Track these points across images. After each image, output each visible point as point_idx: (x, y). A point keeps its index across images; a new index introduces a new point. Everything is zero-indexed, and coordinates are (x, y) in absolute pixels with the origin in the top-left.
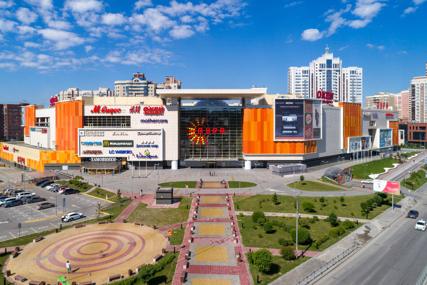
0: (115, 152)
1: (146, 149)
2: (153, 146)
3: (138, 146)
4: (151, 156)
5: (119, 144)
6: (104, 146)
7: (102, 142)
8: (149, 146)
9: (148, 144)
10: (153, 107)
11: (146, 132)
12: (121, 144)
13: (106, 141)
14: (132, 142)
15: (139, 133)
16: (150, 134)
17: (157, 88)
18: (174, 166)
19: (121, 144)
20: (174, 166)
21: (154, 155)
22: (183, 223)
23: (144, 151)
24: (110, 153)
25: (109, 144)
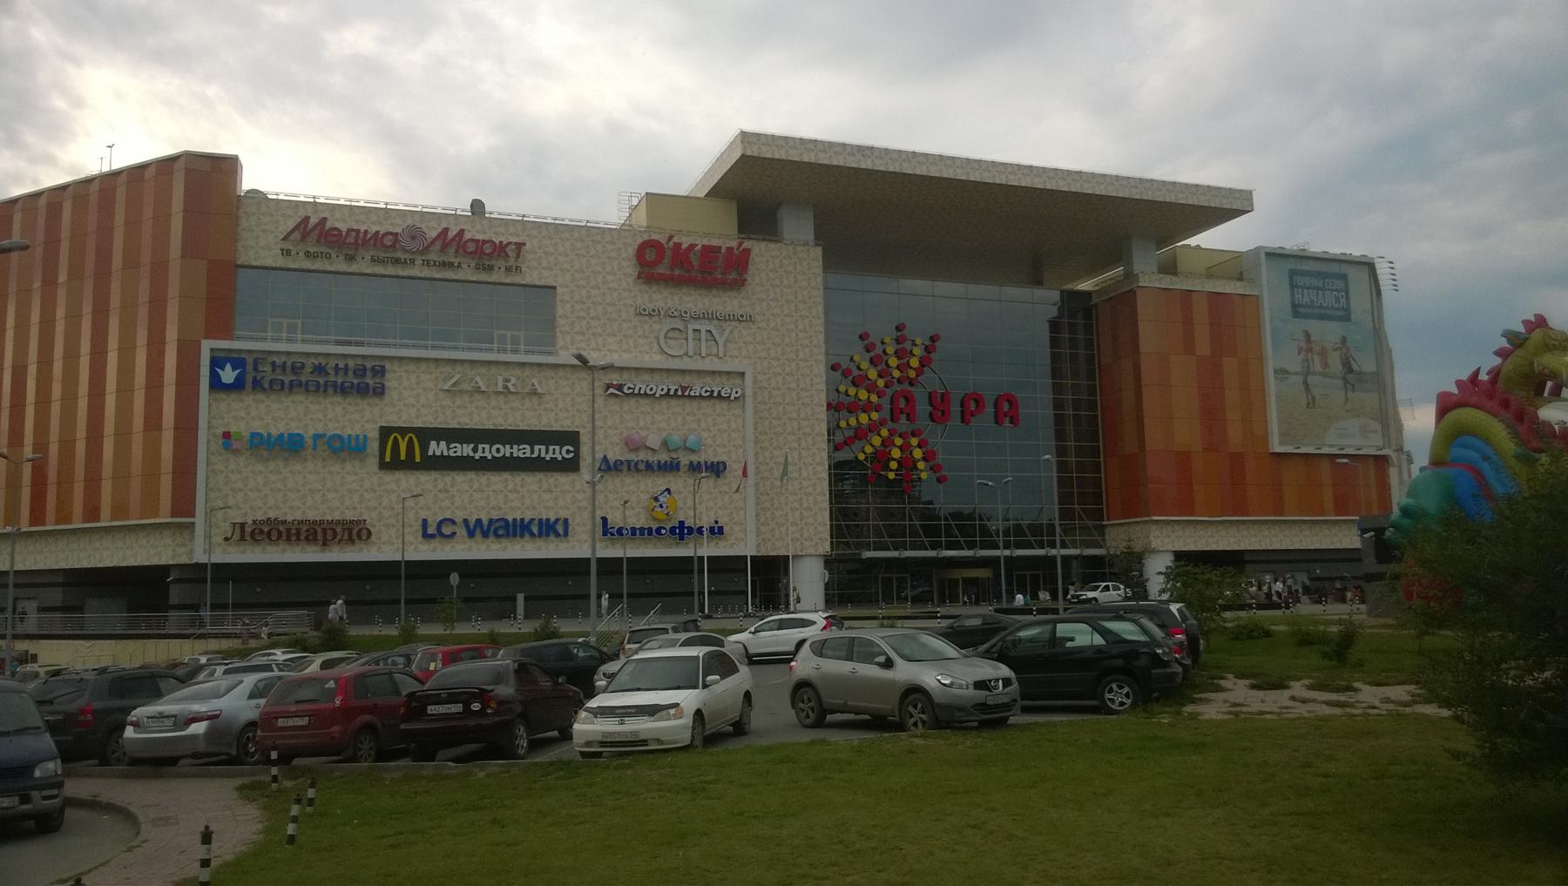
1: (659, 483)
3: (609, 467)
4: (690, 530)
5: (487, 451)
6: (383, 466)
8: (671, 467)
9: (664, 457)
10: (692, 246)
12: (506, 451)
13: (403, 431)
14: (571, 438)
15: (620, 387)
16: (682, 395)
18: (808, 581)
19: (506, 451)
20: (808, 581)
21: (706, 522)
22: (302, 630)
23: (644, 497)
24: (426, 535)
25: (424, 449)
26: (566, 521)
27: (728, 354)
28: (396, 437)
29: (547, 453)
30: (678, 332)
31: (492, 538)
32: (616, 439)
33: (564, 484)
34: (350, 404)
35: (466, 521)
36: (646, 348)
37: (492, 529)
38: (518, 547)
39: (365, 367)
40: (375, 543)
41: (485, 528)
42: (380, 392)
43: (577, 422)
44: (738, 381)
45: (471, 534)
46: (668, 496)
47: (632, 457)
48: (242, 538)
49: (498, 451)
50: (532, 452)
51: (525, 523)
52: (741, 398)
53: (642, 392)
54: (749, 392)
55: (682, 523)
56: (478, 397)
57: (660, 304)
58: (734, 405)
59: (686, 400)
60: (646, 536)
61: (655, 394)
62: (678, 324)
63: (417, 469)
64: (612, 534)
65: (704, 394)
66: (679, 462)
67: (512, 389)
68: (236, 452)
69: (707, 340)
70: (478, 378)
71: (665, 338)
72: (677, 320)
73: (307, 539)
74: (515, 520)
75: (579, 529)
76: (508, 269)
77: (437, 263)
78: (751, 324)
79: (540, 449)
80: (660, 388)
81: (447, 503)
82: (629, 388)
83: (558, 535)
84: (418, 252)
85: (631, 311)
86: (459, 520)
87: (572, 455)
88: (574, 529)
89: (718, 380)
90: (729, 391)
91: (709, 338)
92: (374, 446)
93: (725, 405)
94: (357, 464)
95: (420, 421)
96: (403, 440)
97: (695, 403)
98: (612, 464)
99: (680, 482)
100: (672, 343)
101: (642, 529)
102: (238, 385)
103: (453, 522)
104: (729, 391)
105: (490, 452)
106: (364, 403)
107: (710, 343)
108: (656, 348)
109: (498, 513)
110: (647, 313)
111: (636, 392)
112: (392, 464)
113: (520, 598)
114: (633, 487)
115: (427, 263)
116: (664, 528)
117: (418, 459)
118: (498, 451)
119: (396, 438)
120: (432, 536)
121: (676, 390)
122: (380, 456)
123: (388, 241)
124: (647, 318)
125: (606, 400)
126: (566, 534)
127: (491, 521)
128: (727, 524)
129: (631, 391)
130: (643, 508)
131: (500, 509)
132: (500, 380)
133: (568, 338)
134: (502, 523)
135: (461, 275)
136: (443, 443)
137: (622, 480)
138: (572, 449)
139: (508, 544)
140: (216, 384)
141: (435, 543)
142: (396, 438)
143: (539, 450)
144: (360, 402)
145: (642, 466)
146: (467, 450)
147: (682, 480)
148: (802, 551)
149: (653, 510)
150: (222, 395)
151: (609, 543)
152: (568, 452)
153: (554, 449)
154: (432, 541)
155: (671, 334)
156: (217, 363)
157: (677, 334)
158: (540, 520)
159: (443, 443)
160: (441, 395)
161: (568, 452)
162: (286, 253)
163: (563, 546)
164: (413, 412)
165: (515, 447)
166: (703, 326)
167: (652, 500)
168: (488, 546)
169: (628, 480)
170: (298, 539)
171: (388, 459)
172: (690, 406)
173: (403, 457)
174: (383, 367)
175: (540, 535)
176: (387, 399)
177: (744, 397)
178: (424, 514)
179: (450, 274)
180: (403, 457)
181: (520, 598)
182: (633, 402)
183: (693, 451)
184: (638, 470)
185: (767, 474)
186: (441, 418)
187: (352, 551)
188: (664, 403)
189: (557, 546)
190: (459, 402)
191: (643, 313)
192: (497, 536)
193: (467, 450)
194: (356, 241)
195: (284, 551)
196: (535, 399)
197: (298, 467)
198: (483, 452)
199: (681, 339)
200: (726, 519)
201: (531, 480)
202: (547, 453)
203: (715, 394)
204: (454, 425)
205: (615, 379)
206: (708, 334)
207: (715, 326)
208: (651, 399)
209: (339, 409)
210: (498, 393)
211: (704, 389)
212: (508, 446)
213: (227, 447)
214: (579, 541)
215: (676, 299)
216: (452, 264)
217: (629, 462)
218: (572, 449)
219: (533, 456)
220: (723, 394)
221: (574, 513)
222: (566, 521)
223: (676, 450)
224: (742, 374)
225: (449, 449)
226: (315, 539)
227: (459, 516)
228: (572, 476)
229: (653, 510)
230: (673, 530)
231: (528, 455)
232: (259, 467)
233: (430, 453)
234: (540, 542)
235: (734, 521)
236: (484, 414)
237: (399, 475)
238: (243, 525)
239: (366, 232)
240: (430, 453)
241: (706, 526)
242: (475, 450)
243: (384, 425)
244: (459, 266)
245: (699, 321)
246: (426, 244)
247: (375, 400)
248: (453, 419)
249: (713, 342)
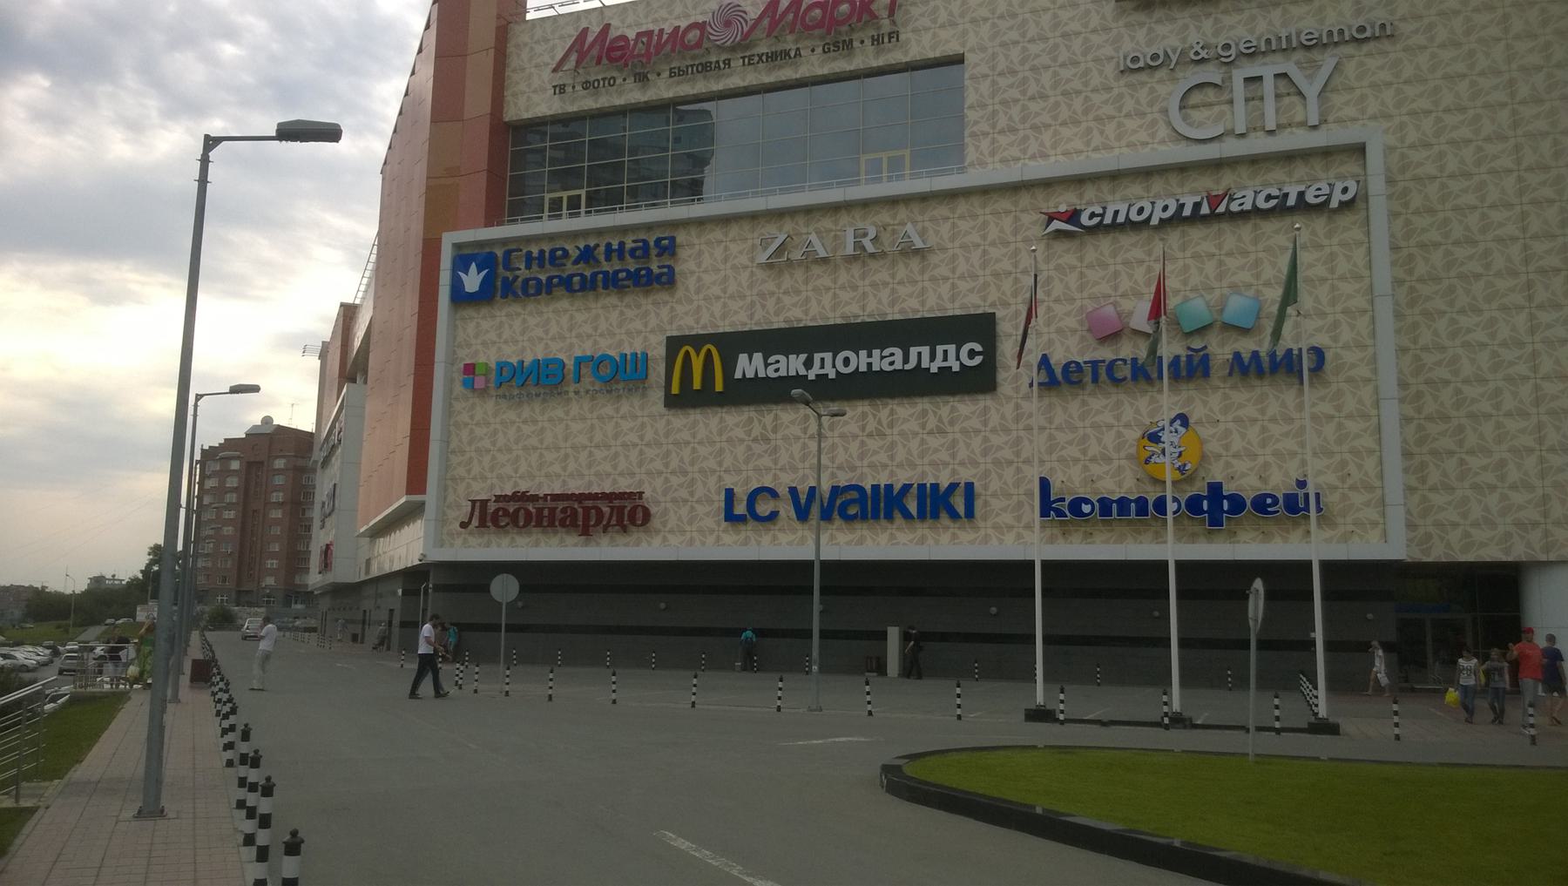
0: (786, 510)
1: (1166, 402)
2: (1246, 369)
4: (1237, 503)
6: (672, 402)
7: (659, 352)
8: (1194, 369)
11: (1158, 202)
12: (860, 361)
13: (697, 341)
14: (981, 327)
15: (1073, 216)
17: (484, 375)
19: (860, 361)
21: (1279, 483)
23: (1134, 434)
24: (731, 517)
25: (729, 366)
26: (969, 487)
27: (1331, 119)
28: (709, 350)
29: (933, 358)
30: (1211, 92)
31: (838, 522)
32: (1071, 322)
33: (967, 418)
34: (630, 307)
35: (793, 491)
36: (1143, 136)
37: (838, 502)
38: (883, 538)
39: (645, 242)
40: (658, 532)
41: (803, 501)
42: (668, 280)
43: (993, 295)
44: (1351, 167)
45: (802, 514)
46: (1182, 430)
47: (1106, 353)
48: (482, 524)
49: (847, 361)
50: (906, 360)
51: (895, 492)
52: (1360, 204)
53: (1121, 219)
54: (1377, 186)
55: (1215, 489)
56: (817, 270)
57: (1174, 42)
58: (1345, 220)
59: (1225, 226)
60: (1133, 516)
61: (1149, 218)
62: (1212, 74)
63: (721, 405)
64: (1060, 513)
65: (1262, 204)
66: (1206, 358)
67: (870, 248)
68: (483, 393)
69: (1278, 96)
70: (813, 237)
71: (1181, 108)
72: (1210, 67)
73: (563, 524)
74: (875, 488)
75: (996, 504)
76: (877, 41)
77: (764, 58)
78: (1386, 45)
79: (920, 354)
80: (1160, 204)
81: (766, 461)
82: (1092, 215)
83: (954, 515)
84: (733, 49)
85: (1110, 69)
86: (783, 491)
87: (978, 360)
88: (986, 503)
89: (1301, 170)
90: (1326, 190)
91: (1283, 90)
92: (658, 371)
93: (1320, 223)
94: (636, 401)
95: (727, 322)
96: (698, 355)
97: (1246, 230)
98: (1058, 371)
99: (1215, 400)
100: (1196, 115)
101: (1123, 503)
102: (484, 296)
103: (773, 493)
104: (1326, 190)
105: (834, 366)
106: (647, 303)
107: (1287, 100)
108: (1163, 132)
109: (851, 475)
110: (1141, 64)
111: (1108, 220)
112: (683, 399)
113: (893, 634)
114: (1107, 417)
115: (749, 62)
116: (1087, 501)
117: (719, 387)
118: (847, 361)
119: (687, 353)
120: (741, 519)
121: (1197, 206)
122: (666, 387)
123: (693, 35)
124: (1143, 77)
125: (1048, 247)
126: (970, 514)
127: (835, 491)
128: (1334, 488)
129: (1096, 220)
130: (1129, 457)
131: (853, 468)
132: (850, 233)
133: (985, 144)
134: (854, 495)
135: (803, 71)
136: (758, 357)
137: (1084, 403)
138: (978, 348)
139: (866, 532)
140: (460, 297)
141: (748, 530)
142: (687, 353)
143: (920, 354)
144: (643, 301)
145: (1125, 371)
146: (793, 365)
147: (1220, 393)
148: (1547, 549)
149: (1147, 461)
150: (469, 312)
151: (1056, 531)
152: (972, 354)
153: (945, 352)
154: (742, 527)
155: (1196, 98)
156: (462, 261)
157: (1211, 94)
158: (922, 487)
159: (758, 357)
160: (760, 274)
161: (972, 354)
162: (560, 89)
163: (966, 536)
164: (717, 308)
165: (876, 352)
166: (1266, 69)
167: (1146, 441)
168: (892, 537)
169: (1097, 403)
170: (552, 524)
171: (675, 390)
172: (1232, 237)
173: (697, 385)
174: (673, 239)
175: (922, 516)
176: (680, 293)
177: (1366, 199)
178: (729, 482)
179: (787, 73)
180: (697, 385)
181: (893, 634)
182: (1105, 243)
183: (1244, 331)
184: (1117, 382)
185: (1443, 373)
186: (705, 319)
187: (626, 545)
188: (1174, 236)
189: (954, 536)
190: (787, 281)
191: (1134, 68)
192: (849, 519)
193: (793, 365)
194: (648, 50)
195: (537, 544)
196: (915, 263)
197: (559, 412)
198: (945, 359)
199: (1219, 103)
200: (1331, 478)
201: (906, 413)
202: (933, 358)
203: (1291, 201)
204: (778, 323)
205: (1063, 202)
206: (1282, 83)
207: (1298, 63)
208: (1145, 234)
209: (614, 316)
210: (853, 259)
211: (1261, 197)
212: (863, 353)
213: (470, 385)
214: (996, 527)
215: (1208, 25)
216: (787, 53)
217: (1095, 364)
218: (978, 348)
219: (907, 367)
220: (1310, 199)
221: (987, 474)
222: (969, 487)
223: (1202, 331)
224: (1359, 150)
225: (767, 365)
226: (574, 525)
227: (783, 483)
228: (984, 401)
229: (1147, 461)
230: (1194, 505)
231: (898, 366)
232: (511, 415)
233: (738, 375)
234: (923, 529)
235: (1349, 482)
236: (885, 295)
237: (695, 415)
238: (484, 503)
239: (661, 31)
240: (738, 375)
241: (1248, 497)
242: (808, 364)
243: (675, 333)
244: (798, 54)
245: (1260, 60)
246: (746, 29)
247: (663, 296)
248: (777, 314)
249: (1295, 99)
